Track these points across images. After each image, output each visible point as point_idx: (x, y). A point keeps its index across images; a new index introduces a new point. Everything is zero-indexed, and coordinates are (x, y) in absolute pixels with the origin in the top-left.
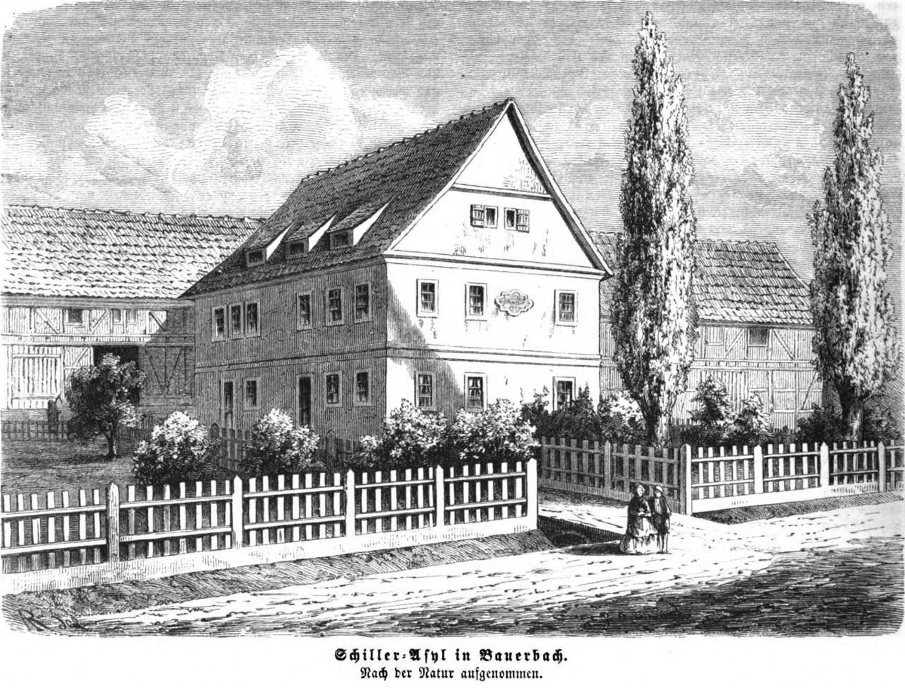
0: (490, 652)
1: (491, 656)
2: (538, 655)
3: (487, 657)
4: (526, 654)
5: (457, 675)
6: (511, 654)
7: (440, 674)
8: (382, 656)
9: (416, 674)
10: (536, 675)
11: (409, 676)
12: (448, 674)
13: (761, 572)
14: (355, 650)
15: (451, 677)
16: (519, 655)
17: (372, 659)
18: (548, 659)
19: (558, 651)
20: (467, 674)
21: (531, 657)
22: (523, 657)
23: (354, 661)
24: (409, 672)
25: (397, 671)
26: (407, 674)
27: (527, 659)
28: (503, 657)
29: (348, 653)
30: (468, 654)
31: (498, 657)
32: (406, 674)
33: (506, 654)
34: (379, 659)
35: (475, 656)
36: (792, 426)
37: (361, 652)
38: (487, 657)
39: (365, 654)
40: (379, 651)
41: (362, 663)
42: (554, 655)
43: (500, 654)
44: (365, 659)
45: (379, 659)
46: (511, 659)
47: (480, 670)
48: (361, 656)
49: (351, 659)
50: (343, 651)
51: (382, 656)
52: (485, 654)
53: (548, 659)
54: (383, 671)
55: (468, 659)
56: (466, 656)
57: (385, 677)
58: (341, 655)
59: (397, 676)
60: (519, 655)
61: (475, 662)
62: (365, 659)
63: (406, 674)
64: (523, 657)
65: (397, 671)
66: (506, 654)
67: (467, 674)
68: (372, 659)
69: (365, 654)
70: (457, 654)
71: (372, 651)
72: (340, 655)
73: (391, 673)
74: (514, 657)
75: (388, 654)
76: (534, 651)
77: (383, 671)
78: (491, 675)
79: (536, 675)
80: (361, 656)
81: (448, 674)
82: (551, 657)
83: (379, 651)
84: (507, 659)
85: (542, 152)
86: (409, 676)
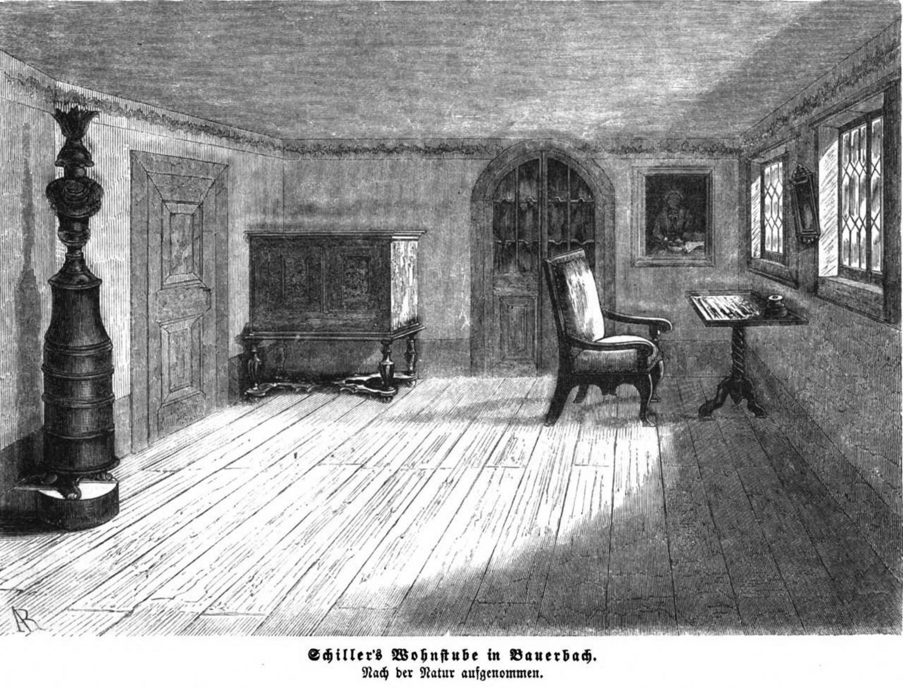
0: (520, 653)
1: (521, 656)
2: (568, 655)
3: (518, 656)
4: (557, 654)
5: (458, 674)
6: (541, 654)
7: (441, 674)
8: (355, 656)
9: (417, 674)
10: (536, 674)
11: (410, 676)
12: (449, 674)
13: (664, 443)
14: (328, 650)
15: (452, 676)
16: (549, 654)
17: (345, 659)
18: (577, 659)
19: (587, 651)
20: (468, 674)
21: (561, 657)
22: (553, 657)
23: (327, 661)
24: (451, 672)
25: (398, 671)
26: (408, 674)
27: (557, 659)
28: (534, 656)
29: (322, 652)
30: (498, 654)
31: (529, 657)
32: (407, 674)
33: (537, 653)
34: (352, 659)
35: (505, 655)
36: (589, 424)
37: (334, 652)
38: (518, 656)
39: (338, 654)
40: (352, 651)
41: (365, 663)
42: (583, 655)
43: (530, 654)
44: (338, 659)
45: (352, 659)
46: (541, 659)
47: (480, 670)
48: (335, 656)
49: (325, 659)
50: (317, 651)
51: (355, 656)
52: (515, 654)
53: (577, 659)
54: (384, 670)
55: (498, 659)
56: (496, 656)
57: (386, 677)
58: (315, 655)
59: (398, 676)
60: (549, 654)
61: (387, 661)
62: (338, 659)
63: (407, 674)
64: (553, 657)
65: (398, 671)
66: (537, 653)
67: (468, 674)
68: (345, 659)
69: (338, 654)
70: (489, 654)
71: (345, 651)
72: (313, 655)
73: (392, 673)
74: (544, 656)
75: (360, 654)
76: (564, 651)
77: (384, 670)
78: (491, 674)
79: (536, 674)
80: (335, 656)
81: (449, 674)
82: (580, 657)
83: (352, 651)
84: (537, 659)
85: (475, 478)
86: (410, 676)
